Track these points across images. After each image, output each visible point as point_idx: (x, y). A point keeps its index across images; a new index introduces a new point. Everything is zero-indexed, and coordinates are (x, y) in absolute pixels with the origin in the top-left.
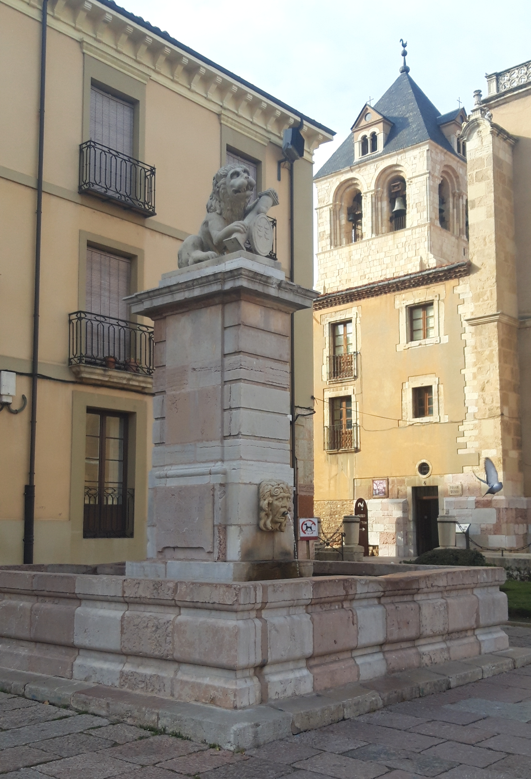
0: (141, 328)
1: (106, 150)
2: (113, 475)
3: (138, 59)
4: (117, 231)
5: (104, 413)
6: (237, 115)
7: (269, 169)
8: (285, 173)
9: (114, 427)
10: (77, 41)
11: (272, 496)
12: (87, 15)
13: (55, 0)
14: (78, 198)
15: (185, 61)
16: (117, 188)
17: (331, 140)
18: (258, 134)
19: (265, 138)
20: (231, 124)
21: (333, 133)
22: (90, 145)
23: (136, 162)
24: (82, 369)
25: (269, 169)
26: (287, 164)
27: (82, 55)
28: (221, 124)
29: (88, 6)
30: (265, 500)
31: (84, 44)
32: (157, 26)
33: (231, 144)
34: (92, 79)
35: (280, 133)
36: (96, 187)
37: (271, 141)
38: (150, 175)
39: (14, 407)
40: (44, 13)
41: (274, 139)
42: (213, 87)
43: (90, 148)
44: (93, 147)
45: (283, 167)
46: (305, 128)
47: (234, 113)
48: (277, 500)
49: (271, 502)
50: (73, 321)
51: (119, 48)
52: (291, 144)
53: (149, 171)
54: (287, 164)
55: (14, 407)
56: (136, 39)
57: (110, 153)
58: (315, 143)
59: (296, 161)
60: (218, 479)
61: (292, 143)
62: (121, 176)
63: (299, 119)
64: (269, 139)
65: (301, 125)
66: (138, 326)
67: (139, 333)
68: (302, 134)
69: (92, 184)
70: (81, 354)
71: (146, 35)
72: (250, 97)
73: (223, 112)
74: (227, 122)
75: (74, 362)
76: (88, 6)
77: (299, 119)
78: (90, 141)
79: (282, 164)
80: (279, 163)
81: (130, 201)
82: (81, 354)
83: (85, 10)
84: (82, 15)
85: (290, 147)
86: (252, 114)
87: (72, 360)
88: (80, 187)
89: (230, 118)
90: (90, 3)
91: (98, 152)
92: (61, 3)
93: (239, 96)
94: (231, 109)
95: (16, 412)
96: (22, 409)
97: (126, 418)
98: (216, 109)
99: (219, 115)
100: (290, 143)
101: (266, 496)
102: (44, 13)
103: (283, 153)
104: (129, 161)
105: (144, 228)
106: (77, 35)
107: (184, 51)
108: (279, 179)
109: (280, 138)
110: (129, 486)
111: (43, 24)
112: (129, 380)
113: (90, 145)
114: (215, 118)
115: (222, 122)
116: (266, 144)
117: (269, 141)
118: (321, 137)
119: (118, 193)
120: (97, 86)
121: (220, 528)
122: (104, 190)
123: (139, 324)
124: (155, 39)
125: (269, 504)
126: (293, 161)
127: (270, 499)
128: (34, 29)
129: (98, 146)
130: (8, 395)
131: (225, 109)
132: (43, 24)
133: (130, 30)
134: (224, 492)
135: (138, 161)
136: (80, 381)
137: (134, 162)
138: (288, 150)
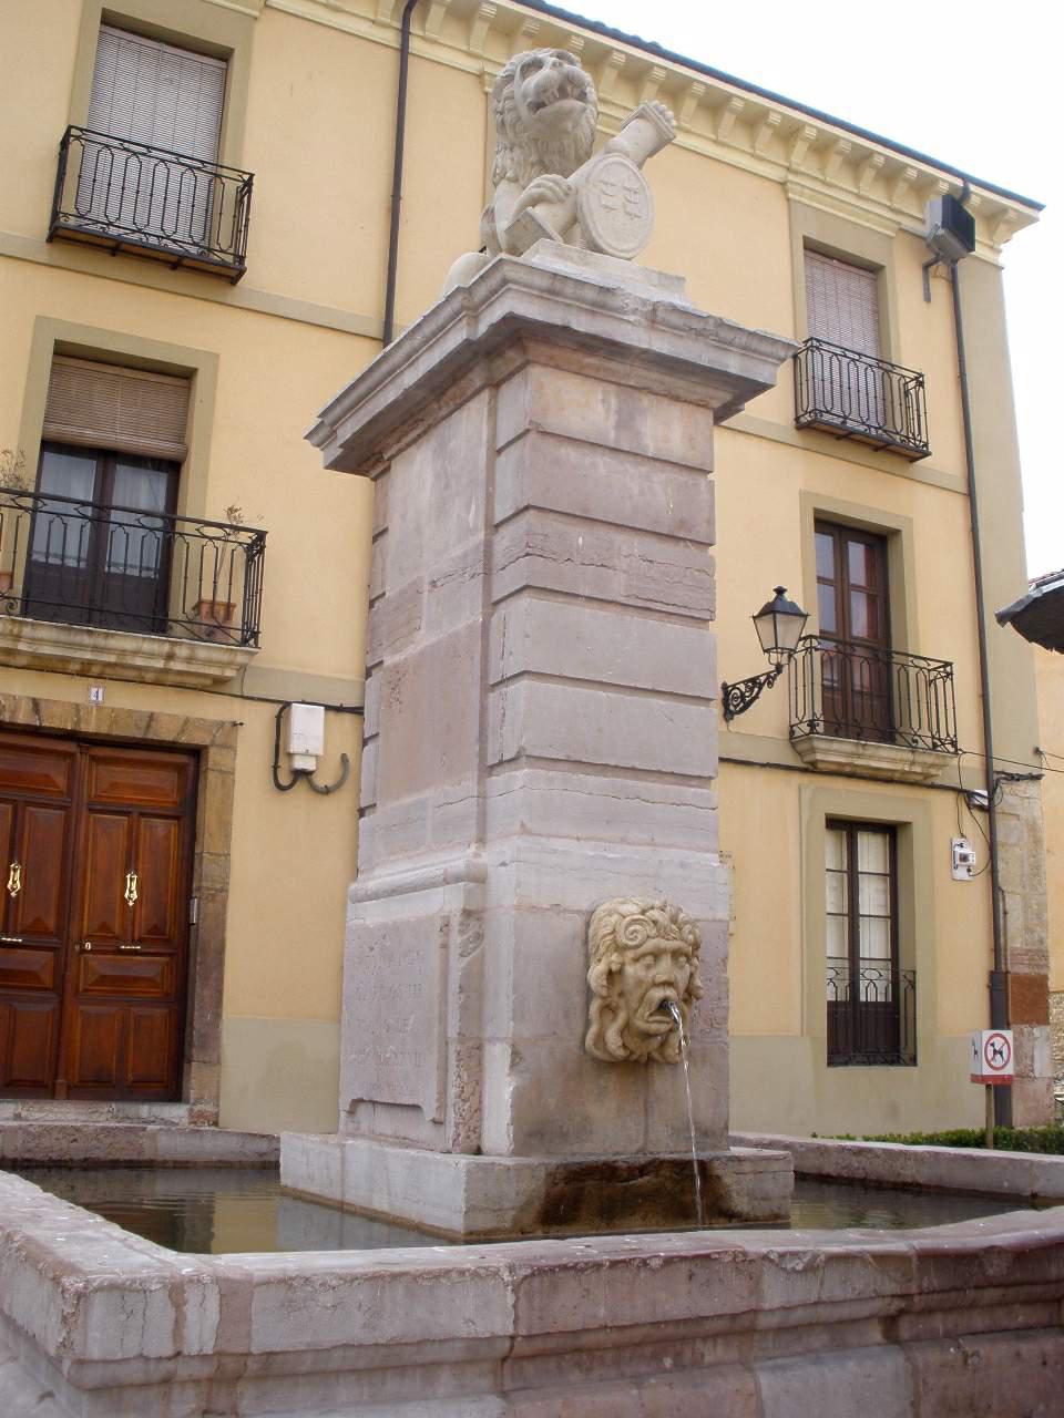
0: (916, 662)
1: (838, 351)
2: (874, 943)
3: (721, 138)
4: (864, 492)
5: (846, 828)
6: (824, 183)
7: (904, 281)
8: (940, 289)
9: (871, 853)
10: (774, 181)
11: (621, 949)
12: (619, 75)
13: (427, 2)
14: (794, 437)
15: (810, 133)
16: (861, 413)
17: (1033, 220)
18: (872, 216)
19: (888, 223)
20: (811, 198)
21: (1038, 207)
22: (812, 346)
23: (890, 368)
24: (817, 744)
25: (904, 281)
26: (942, 269)
27: (483, 97)
28: (788, 200)
29: (487, 10)
30: (600, 960)
31: (486, 77)
32: (657, 40)
33: (814, 236)
34: (805, 238)
35: (922, 212)
36: (826, 417)
37: (902, 226)
38: (915, 388)
39: (322, 780)
40: (405, 33)
41: (907, 223)
42: (869, 174)
43: (812, 351)
44: (818, 348)
45: (935, 276)
46: (974, 200)
47: (816, 179)
48: (636, 960)
49: (615, 968)
50: (796, 656)
51: (862, 193)
52: (943, 227)
53: (913, 380)
54: (942, 269)
55: (322, 780)
56: (857, 162)
57: (845, 356)
58: (1002, 228)
59: (961, 261)
60: (449, 901)
61: (944, 225)
62: (193, 206)
63: (959, 182)
64: (899, 223)
65: (966, 193)
66: (911, 659)
67: (913, 672)
68: (970, 212)
69: (821, 411)
70: (814, 714)
71: (907, 165)
72: (912, 174)
73: (791, 177)
74: (801, 195)
75: (798, 733)
76: (487, 10)
77: (959, 182)
78: (811, 339)
79: (932, 269)
80: (926, 267)
81: (885, 436)
82: (814, 714)
83: (483, 19)
84: (481, 29)
85: (941, 232)
86: (857, 179)
87: (794, 728)
88: (797, 419)
89: (808, 188)
90: (492, 4)
91: (827, 356)
92: (436, 13)
93: (822, 148)
94: (912, 213)
95: (327, 791)
96: (339, 785)
97: (891, 831)
98: (777, 174)
99: (783, 184)
100: (940, 224)
101: (602, 949)
102: (405, 33)
103: (928, 246)
104: (879, 367)
105: (912, 483)
106: (473, 65)
107: (576, 27)
108: (928, 299)
109: (922, 221)
110: (904, 965)
111: (404, 52)
112: (852, 755)
113: (812, 346)
114: (775, 191)
115: (790, 195)
116: (892, 234)
117: (897, 226)
118: (1011, 215)
119: (863, 423)
120: (813, 249)
121: (655, 1043)
122: (841, 420)
123: (912, 656)
124: (631, 55)
125: (612, 976)
126: (955, 261)
127: (614, 957)
128: (390, 60)
129: (825, 347)
130: (307, 754)
131: (796, 173)
132: (404, 52)
133: (620, 59)
134: (479, 937)
135: (893, 366)
136: (812, 769)
137: (885, 367)
138: (936, 239)
